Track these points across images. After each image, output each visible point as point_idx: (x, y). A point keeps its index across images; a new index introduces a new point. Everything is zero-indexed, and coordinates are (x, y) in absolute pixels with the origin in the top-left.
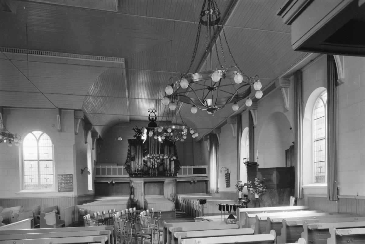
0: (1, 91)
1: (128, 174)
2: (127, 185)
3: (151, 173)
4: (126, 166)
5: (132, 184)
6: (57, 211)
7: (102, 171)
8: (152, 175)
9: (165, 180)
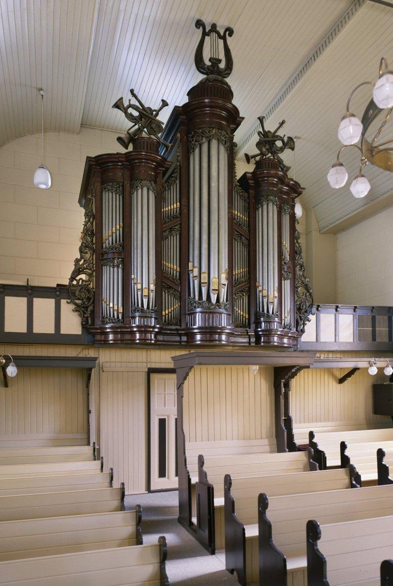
3: (204, 330)
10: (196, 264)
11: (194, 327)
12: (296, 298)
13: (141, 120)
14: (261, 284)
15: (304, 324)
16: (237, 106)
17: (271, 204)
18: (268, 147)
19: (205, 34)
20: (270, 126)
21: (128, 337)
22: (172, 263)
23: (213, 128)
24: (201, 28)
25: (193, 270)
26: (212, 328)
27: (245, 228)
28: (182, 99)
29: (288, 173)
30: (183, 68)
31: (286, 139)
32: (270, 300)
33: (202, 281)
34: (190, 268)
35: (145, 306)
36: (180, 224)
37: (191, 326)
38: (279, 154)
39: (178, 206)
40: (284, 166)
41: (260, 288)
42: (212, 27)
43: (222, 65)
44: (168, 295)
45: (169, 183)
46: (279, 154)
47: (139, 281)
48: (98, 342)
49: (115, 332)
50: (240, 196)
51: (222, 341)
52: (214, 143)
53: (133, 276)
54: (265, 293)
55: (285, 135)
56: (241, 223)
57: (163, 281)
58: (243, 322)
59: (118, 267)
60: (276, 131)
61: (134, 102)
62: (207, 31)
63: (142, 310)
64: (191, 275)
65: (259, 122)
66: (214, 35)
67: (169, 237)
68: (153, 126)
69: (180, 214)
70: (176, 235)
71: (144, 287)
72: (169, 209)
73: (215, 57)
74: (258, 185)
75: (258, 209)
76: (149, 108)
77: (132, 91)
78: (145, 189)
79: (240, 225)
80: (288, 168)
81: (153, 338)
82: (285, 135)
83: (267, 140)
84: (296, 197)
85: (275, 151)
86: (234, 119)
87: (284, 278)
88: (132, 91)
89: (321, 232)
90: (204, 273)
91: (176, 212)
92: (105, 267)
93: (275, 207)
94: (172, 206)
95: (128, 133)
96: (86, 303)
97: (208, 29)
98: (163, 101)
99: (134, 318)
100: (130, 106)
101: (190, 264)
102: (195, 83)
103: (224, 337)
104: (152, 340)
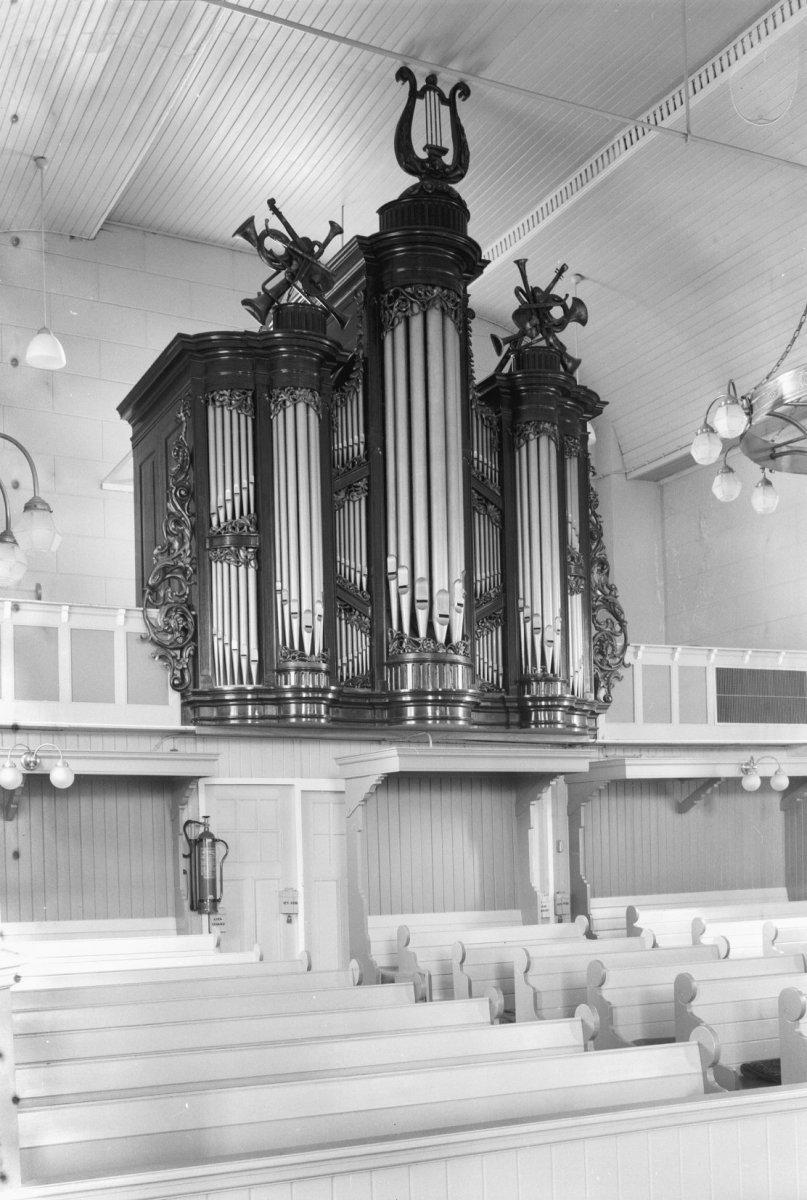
0: (45, 2)
1: (175, 698)
2: (152, 808)
3: (419, 697)
4: (154, 613)
5: (200, 805)
6: (499, 1002)
7: (682, 688)
8: (421, 717)
9: (212, 758)
10: (405, 560)
11: (403, 691)
12: (594, 632)
13: (291, 264)
14: (528, 603)
15: (609, 686)
16: (476, 239)
17: (544, 440)
18: (535, 321)
19: (414, 95)
20: (539, 279)
21: (272, 710)
22: (352, 559)
23: (434, 287)
24: (408, 83)
25: (396, 573)
26: (445, 693)
27: (495, 487)
28: (368, 225)
29: (577, 374)
30: (355, 139)
31: (569, 303)
32: (547, 637)
33: (417, 597)
34: (391, 568)
35: (307, 650)
36: (369, 478)
37: (397, 688)
38: (557, 334)
39: (362, 439)
40: (570, 359)
41: (527, 612)
42: (427, 80)
43: (448, 159)
44: (346, 624)
45: (343, 391)
46: (557, 334)
47: (294, 595)
48: (207, 723)
49: (418, 701)
50: (483, 422)
51: (458, 719)
52: (434, 317)
53: (278, 586)
54: (537, 622)
55: (567, 295)
56: (485, 475)
57: (339, 597)
58: (493, 682)
59: (247, 564)
60: (550, 288)
61: (276, 224)
62: (419, 89)
63: (302, 656)
64: (393, 585)
65: (516, 267)
66: (432, 96)
67: (346, 504)
68: (317, 278)
69: (367, 456)
70: (360, 500)
71: (304, 608)
72: (345, 445)
73: (434, 143)
74: (516, 399)
75: (519, 449)
76: (306, 240)
77: (271, 203)
78: (301, 407)
79: (483, 477)
80: (577, 363)
81: (323, 713)
82: (567, 295)
83: (535, 306)
84: (590, 419)
85: (550, 328)
86: (472, 261)
87: (571, 589)
88: (271, 203)
89: (630, 476)
90: (422, 579)
91: (359, 453)
92: (219, 564)
93: (553, 444)
94: (352, 439)
95: (264, 289)
96: (180, 640)
97: (421, 84)
98: (332, 223)
99: (285, 671)
100: (269, 232)
101: (391, 561)
102: (394, 195)
103: (461, 712)
104: (320, 717)
